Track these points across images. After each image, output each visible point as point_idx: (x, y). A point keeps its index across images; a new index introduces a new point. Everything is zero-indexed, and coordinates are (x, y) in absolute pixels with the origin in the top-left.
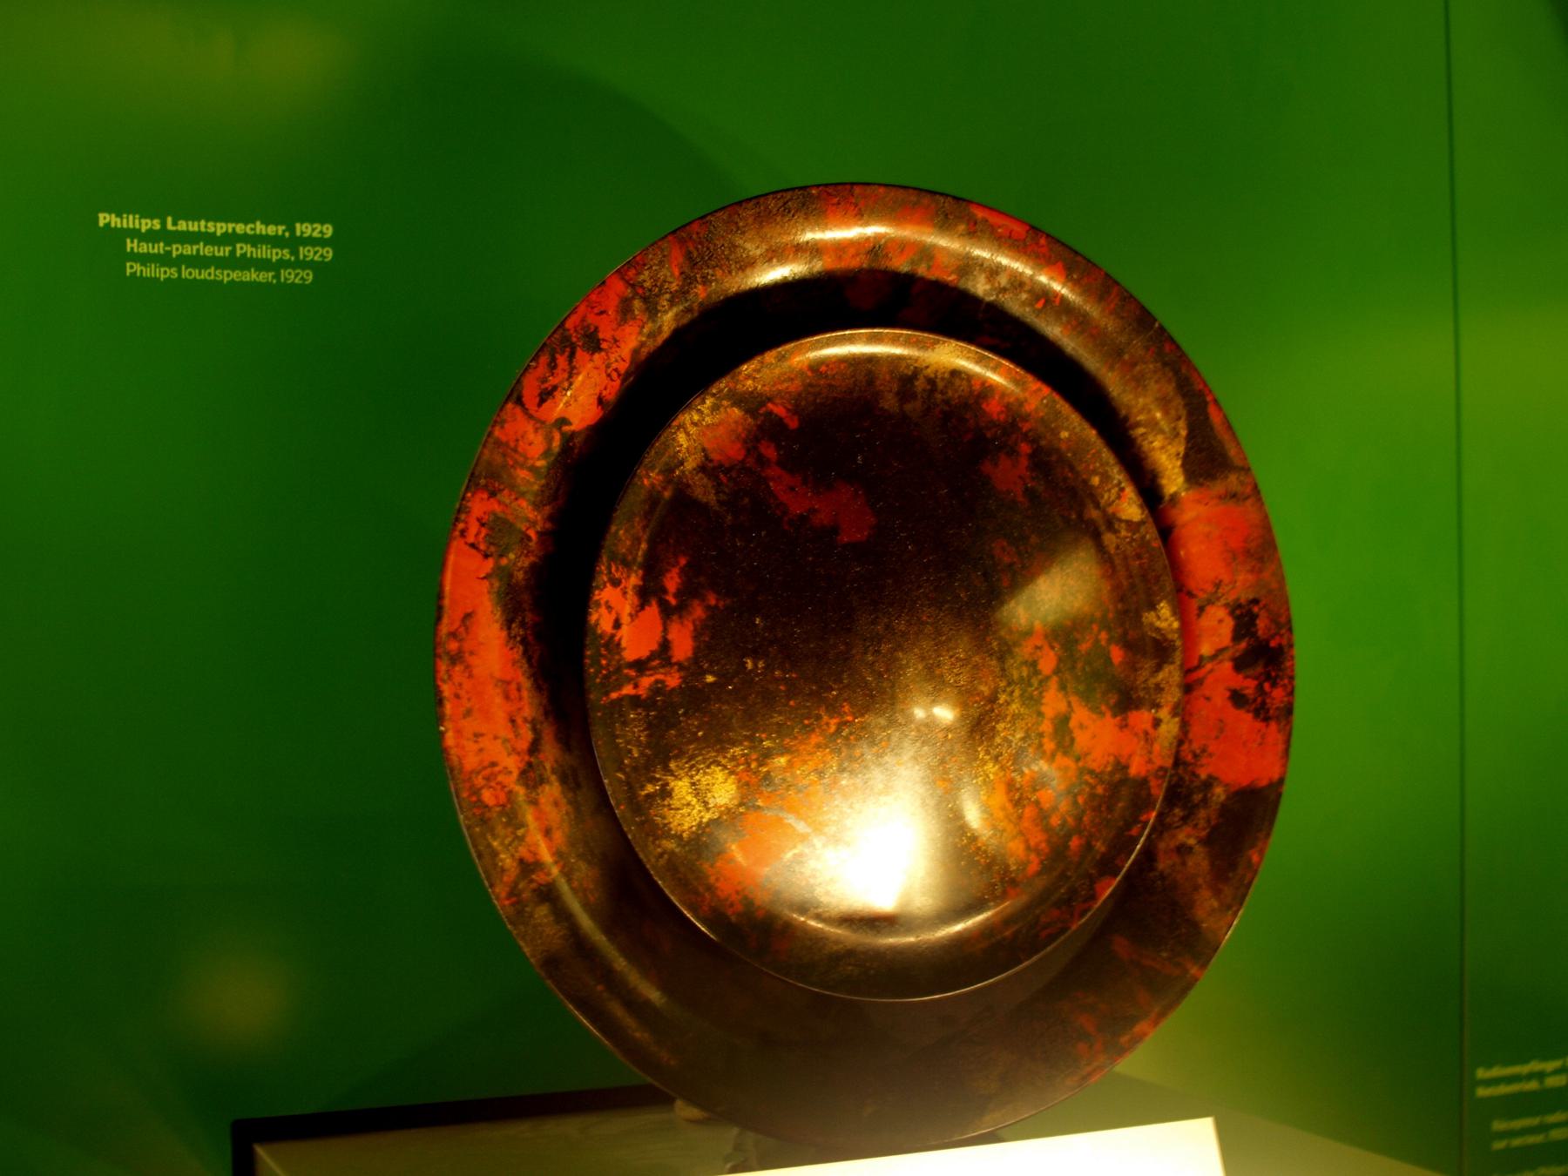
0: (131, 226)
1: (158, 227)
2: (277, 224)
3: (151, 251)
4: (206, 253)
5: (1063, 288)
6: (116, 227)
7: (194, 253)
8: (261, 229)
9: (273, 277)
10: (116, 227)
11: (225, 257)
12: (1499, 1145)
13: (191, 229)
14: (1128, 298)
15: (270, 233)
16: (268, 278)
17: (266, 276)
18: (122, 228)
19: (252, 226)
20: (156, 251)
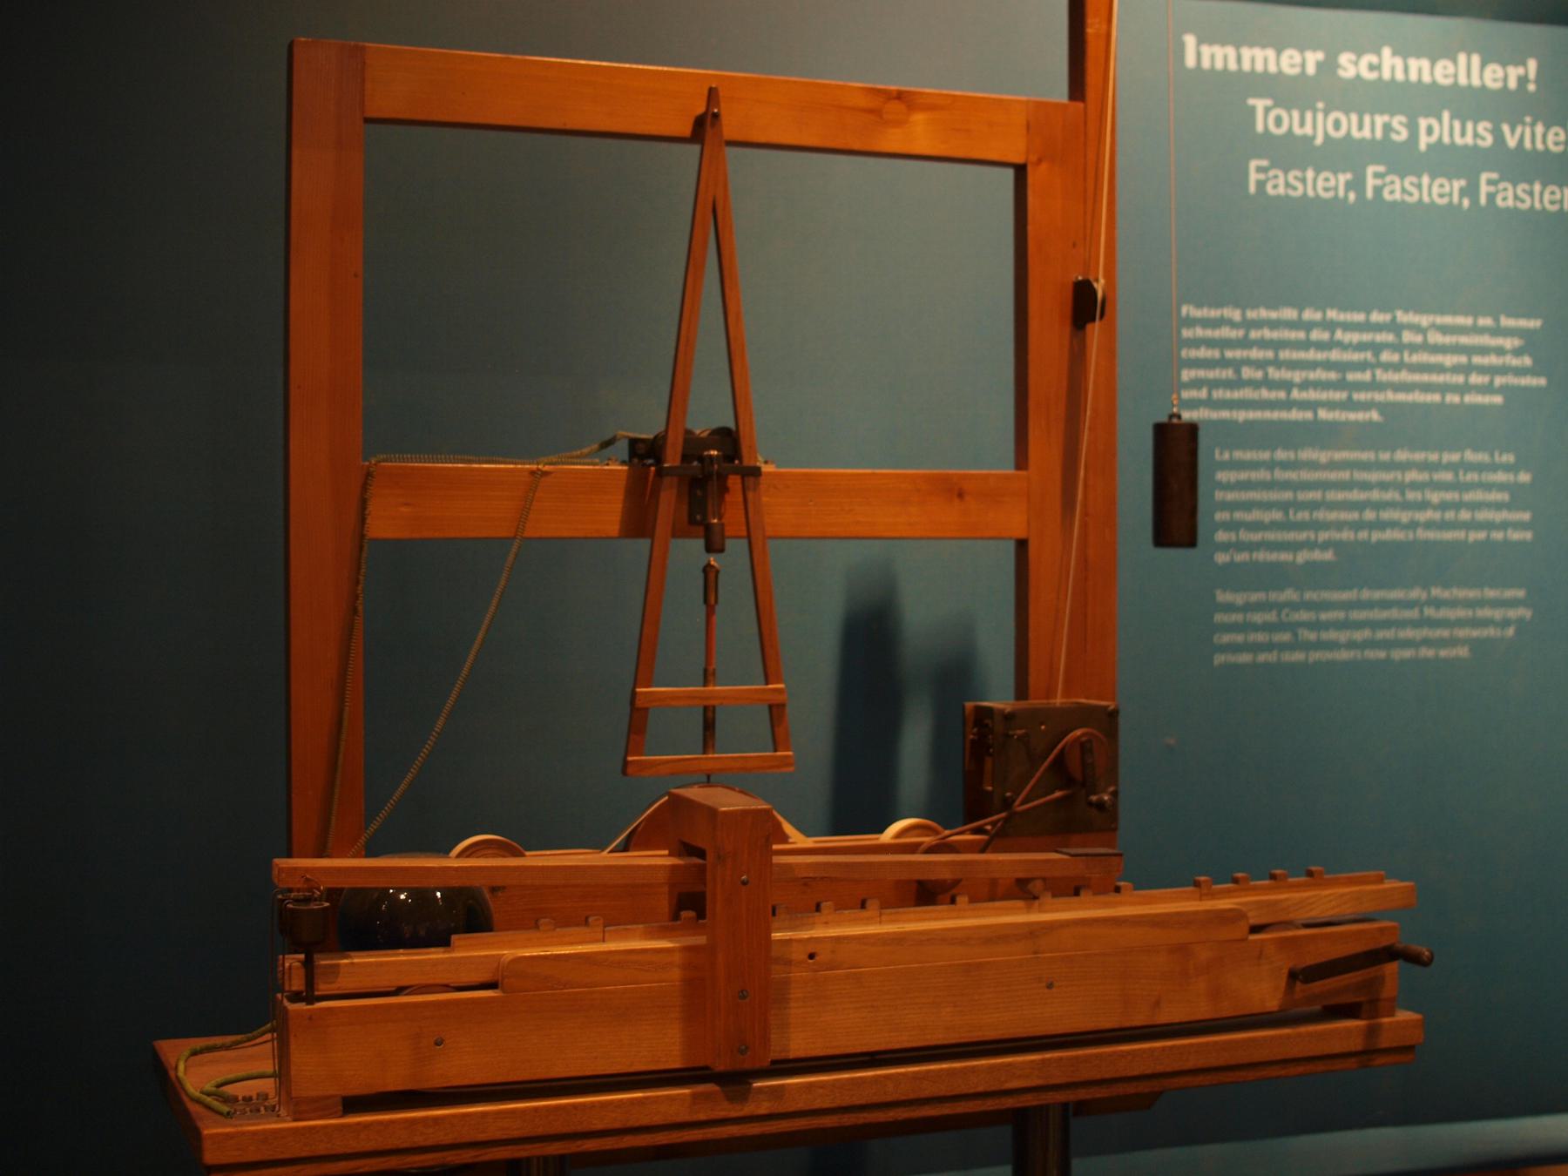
0: (1476, 82)
1: (1345, 59)
2: (1302, 49)
3: (1458, 140)
4: (1552, 147)
5: (1347, 419)
6: (1420, 81)
7: (1379, 134)
8: (1393, 69)
9: (1349, 186)
10: (1253, 70)
11: (1373, 139)
12: (1219, 659)
13: (1230, 51)
14: (706, 601)
15: (1288, 70)
16: (1336, 189)
17: (1447, 189)
18: (1470, 87)
19: (1373, 59)
20: (1366, 133)
